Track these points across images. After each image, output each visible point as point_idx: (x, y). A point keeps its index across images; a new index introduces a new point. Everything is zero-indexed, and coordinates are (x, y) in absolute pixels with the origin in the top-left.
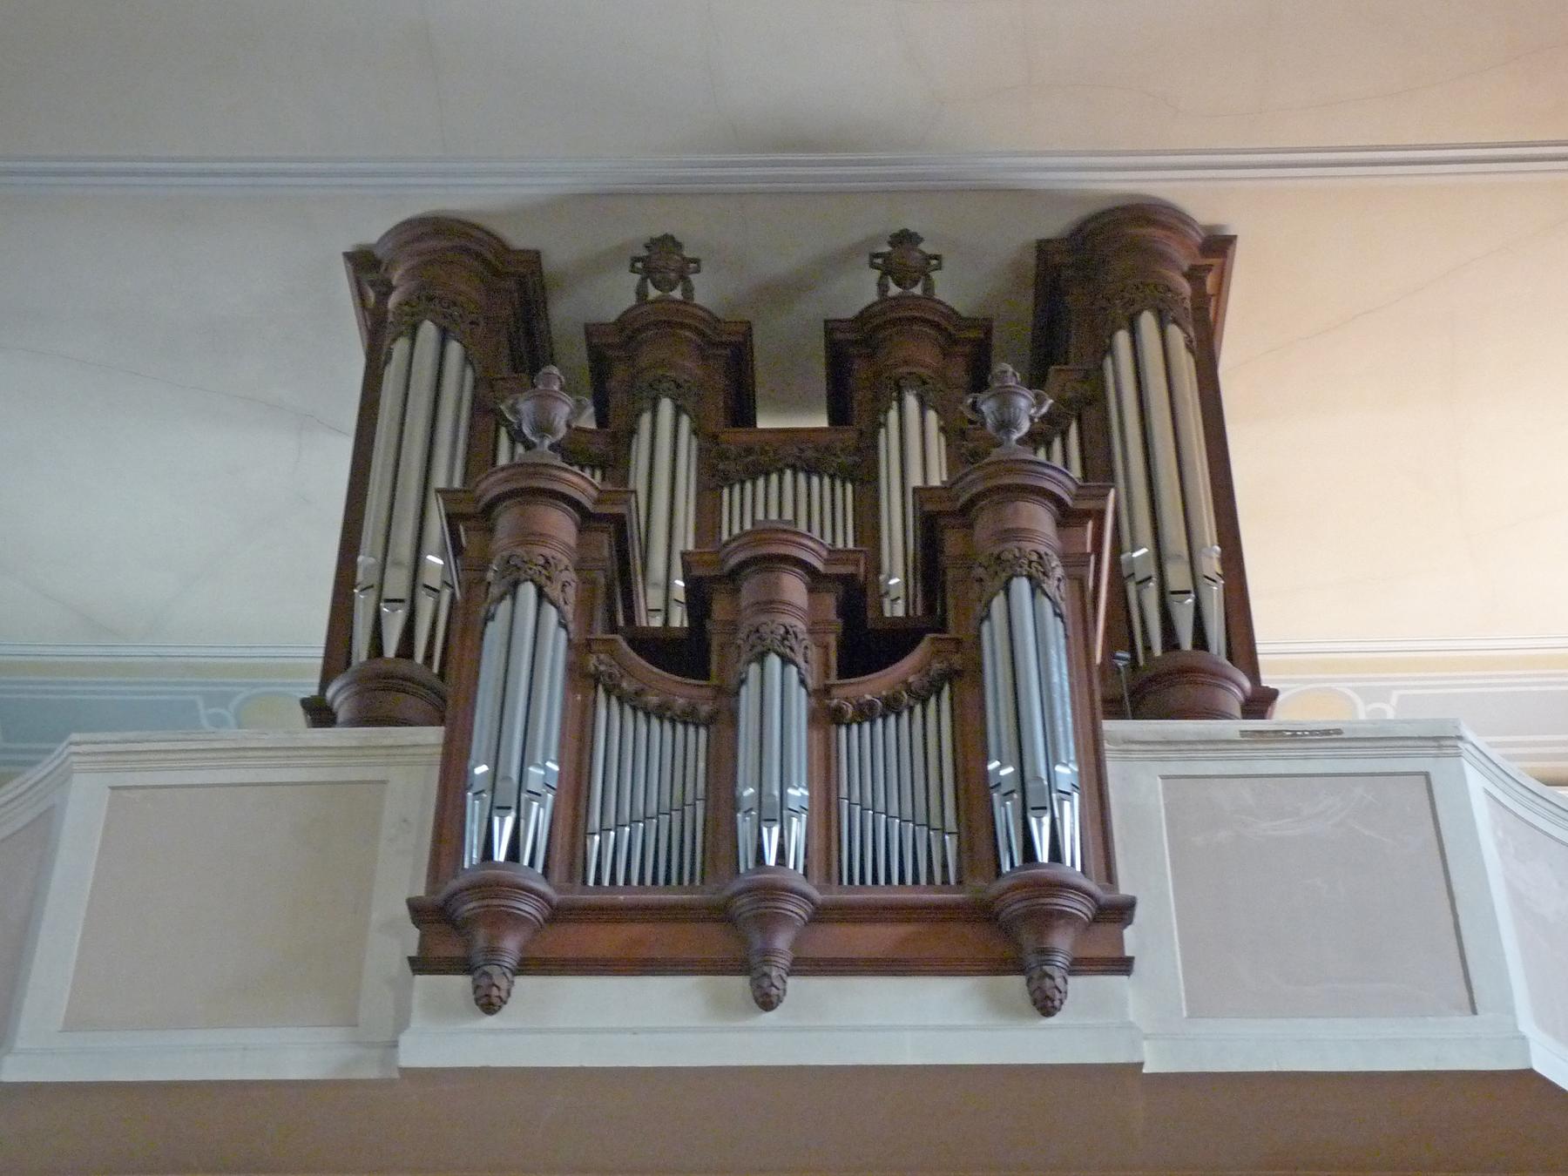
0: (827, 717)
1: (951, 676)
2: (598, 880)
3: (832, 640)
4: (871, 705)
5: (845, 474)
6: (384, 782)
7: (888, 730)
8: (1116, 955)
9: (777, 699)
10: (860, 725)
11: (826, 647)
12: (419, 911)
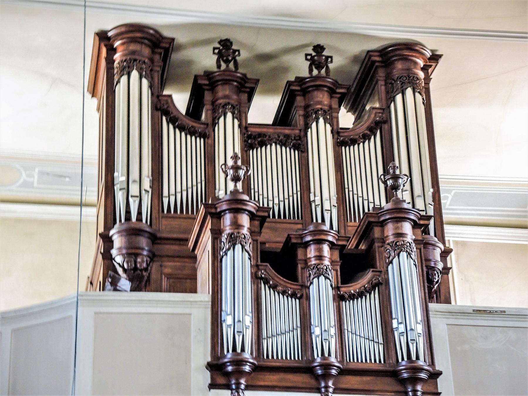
0: (340, 298)
1: (378, 284)
2: (268, 356)
3: (338, 268)
4: (354, 295)
5: (296, 147)
6: (190, 314)
7: (358, 303)
8: (434, 391)
9: (322, 290)
10: (349, 301)
11: (337, 271)
12: (210, 366)
